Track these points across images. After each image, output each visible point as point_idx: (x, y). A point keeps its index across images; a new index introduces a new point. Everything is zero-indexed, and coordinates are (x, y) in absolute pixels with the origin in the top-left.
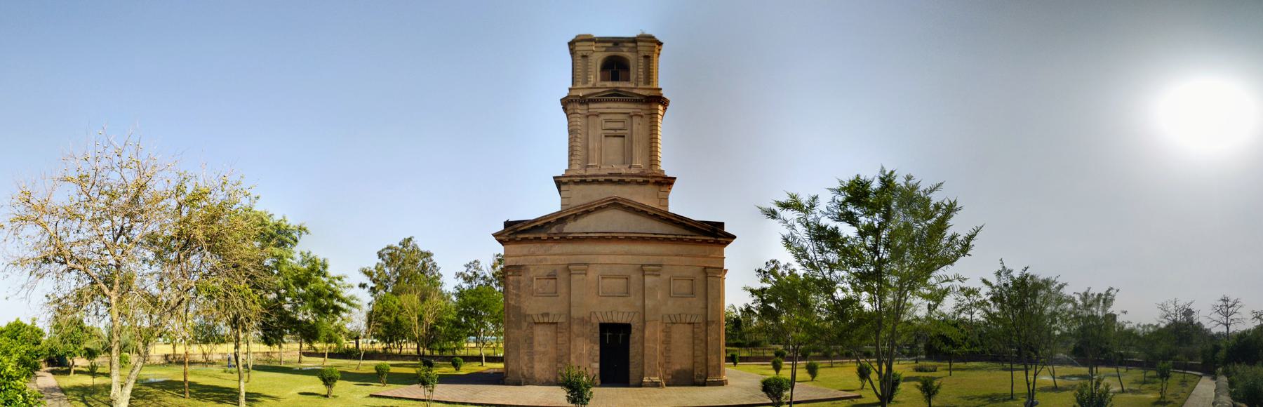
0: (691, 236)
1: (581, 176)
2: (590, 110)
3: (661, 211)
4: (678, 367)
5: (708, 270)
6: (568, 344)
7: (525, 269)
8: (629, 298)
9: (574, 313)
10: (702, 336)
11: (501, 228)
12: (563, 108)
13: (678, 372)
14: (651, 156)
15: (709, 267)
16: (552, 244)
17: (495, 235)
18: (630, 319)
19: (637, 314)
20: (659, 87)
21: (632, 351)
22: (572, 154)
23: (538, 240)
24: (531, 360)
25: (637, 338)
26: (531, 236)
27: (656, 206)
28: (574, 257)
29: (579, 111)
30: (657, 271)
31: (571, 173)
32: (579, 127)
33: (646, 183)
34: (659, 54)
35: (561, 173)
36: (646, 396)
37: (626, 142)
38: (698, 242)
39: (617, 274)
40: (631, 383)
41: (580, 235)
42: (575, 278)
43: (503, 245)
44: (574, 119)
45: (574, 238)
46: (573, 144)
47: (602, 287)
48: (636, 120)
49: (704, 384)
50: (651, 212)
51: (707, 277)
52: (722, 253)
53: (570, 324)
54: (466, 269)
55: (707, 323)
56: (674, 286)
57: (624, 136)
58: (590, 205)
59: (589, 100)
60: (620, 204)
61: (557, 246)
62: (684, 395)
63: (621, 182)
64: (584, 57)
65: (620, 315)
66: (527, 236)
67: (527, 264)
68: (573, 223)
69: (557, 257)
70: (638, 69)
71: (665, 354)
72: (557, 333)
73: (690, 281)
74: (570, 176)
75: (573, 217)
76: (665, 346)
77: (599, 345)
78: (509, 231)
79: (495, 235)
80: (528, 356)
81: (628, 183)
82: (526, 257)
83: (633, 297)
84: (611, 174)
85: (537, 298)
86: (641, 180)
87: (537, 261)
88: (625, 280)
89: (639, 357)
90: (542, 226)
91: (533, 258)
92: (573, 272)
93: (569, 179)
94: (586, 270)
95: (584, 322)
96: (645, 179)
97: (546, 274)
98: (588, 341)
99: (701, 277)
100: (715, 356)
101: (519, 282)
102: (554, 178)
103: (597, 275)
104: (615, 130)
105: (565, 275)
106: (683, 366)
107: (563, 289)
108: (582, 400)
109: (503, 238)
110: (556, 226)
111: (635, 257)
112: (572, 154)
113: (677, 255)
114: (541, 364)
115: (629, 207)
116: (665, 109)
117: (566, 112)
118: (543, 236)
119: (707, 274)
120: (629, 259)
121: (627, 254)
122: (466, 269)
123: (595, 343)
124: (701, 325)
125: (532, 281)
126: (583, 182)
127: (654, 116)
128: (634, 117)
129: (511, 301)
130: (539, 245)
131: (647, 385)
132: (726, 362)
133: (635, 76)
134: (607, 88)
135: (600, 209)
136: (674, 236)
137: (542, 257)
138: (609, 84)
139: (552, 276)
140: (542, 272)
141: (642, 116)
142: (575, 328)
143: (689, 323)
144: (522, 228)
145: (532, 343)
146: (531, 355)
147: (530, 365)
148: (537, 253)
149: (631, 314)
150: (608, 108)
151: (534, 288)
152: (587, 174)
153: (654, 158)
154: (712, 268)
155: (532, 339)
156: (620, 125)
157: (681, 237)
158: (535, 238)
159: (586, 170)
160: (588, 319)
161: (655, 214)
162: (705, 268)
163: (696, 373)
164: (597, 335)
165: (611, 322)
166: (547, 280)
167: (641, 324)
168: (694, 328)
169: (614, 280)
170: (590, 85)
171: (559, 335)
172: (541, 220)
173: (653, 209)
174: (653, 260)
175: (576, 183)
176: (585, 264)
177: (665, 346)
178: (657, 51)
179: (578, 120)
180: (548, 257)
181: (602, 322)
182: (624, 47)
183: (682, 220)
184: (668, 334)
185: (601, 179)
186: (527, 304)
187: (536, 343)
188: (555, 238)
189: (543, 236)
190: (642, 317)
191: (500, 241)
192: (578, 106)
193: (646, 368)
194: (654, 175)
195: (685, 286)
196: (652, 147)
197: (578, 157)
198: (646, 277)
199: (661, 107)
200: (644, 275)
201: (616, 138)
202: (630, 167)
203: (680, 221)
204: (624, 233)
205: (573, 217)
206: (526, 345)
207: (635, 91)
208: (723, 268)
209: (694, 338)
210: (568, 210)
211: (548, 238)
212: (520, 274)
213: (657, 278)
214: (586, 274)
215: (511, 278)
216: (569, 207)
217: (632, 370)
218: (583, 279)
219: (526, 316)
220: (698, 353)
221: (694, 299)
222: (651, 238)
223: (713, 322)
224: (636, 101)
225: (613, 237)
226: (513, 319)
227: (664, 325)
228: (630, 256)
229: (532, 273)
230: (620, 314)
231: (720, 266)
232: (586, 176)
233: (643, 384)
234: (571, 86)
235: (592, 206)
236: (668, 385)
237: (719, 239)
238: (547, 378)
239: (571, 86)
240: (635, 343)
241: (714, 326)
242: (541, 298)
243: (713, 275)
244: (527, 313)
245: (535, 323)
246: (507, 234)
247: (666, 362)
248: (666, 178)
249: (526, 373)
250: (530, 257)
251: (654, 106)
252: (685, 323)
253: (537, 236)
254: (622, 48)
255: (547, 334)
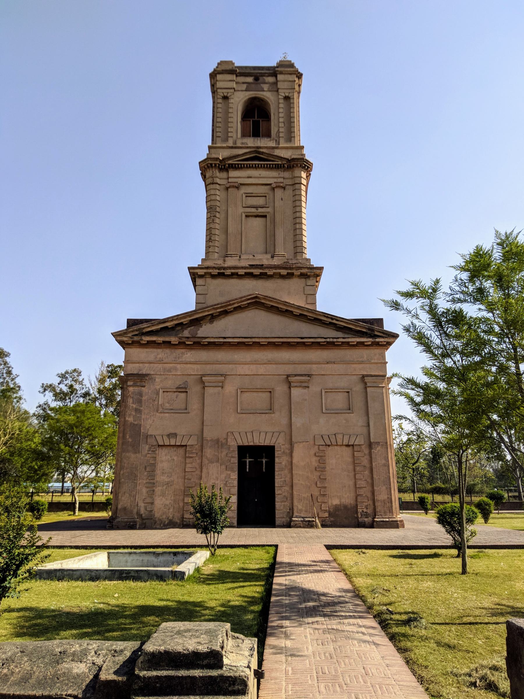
0: (343, 338)
1: (219, 268)
2: (230, 180)
3: (308, 310)
4: (336, 502)
5: (367, 379)
6: (198, 472)
7: (150, 379)
8: (273, 415)
9: (208, 434)
10: (365, 461)
11: (123, 326)
12: (202, 174)
13: (337, 508)
14: (295, 235)
15: (368, 376)
16: (183, 350)
17: (115, 335)
18: (274, 440)
19: (282, 434)
20: (301, 145)
21: (278, 481)
22: (210, 239)
23: (167, 344)
24: (152, 493)
25: (283, 463)
26: (160, 339)
27: (302, 304)
28: (208, 366)
29: (218, 181)
30: (305, 382)
31: (209, 264)
32: (218, 204)
33: (290, 276)
34: (299, 93)
35: (196, 262)
36: (295, 535)
37: (268, 223)
38: (353, 346)
39: (259, 387)
40: (278, 522)
41: (216, 340)
42: (209, 391)
43: (124, 348)
44: (212, 192)
45: (210, 343)
46: (212, 226)
47: (241, 402)
48: (279, 193)
49: (372, 526)
50: (297, 312)
51: (366, 388)
52: (384, 357)
53: (202, 446)
54: (59, 379)
55: (370, 445)
56: (326, 399)
57: (265, 216)
58: (228, 303)
59: (229, 164)
60: (263, 303)
61: (189, 354)
62: (344, 535)
63: (263, 276)
64: (225, 98)
65: (263, 435)
66: (154, 338)
67: (152, 373)
68: (209, 326)
69: (189, 366)
70: (279, 117)
71: (319, 485)
72: (186, 458)
73: (346, 394)
74: (207, 268)
75: (209, 318)
76: (318, 474)
77: (237, 472)
78: (133, 331)
79: (115, 335)
80: (147, 487)
81: (271, 277)
82: (152, 365)
83: (277, 414)
84: (252, 266)
85: (162, 415)
86: (284, 272)
87: (165, 369)
88: (268, 394)
89: (287, 488)
90: (173, 328)
91: (160, 366)
92: (206, 384)
93: (205, 271)
94: (222, 382)
95: (218, 444)
96: (289, 271)
97: (176, 386)
98: (223, 467)
99: (358, 388)
100: (384, 488)
101: (141, 394)
102: (189, 268)
103: (235, 388)
104: (256, 207)
105: (198, 388)
106: (343, 500)
107: (194, 405)
108: (215, 528)
109: (125, 339)
110: (189, 329)
111: (280, 366)
112: (210, 239)
113: (328, 363)
114: (164, 499)
115: (272, 306)
116: (308, 177)
117: (204, 181)
118: (174, 340)
119: (366, 384)
120: (272, 369)
121: (269, 362)
122: (59, 379)
123: (232, 470)
124: (363, 447)
125: (158, 394)
126: (221, 275)
127: (297, 186)
128: (276, 190)
129: (129, 417)
130: (168, 351)
131: (296, 526)
132: (400, 510)
133: (276, 130)
134: (248, 148)
135: (239, 309)
136: (323, 340)
137: (171, 365)
138: (251, 142)
139: (182, 389)
140: (170, 383)
141: (284, 188)
142: (209, 452)
143: (348, 446)
144: (149, 329)
145: (154, 471)
146: (152, 486)
147: (149, 500)
148: (165, 361)
149: (276, 434)
150: (248, 177)
151: (160, 403)
152: (226, 266)
153: (298, 244)
154: (372, 376)
155: (154, 465)
156: (261, 201)
157: (331, 340)
158: (164, 342)
159: (225, 261)
160: (224, 441)
161: (301, 315)
162: (363, 376)
163: (360, 510)
164: (235, 460)
165: (251, 444)
166: (176, 394)
167: (287, 446)
168: (354, 451)
169: (255, 394)
170: (230, 143)
171: (188, 460)
172: (172, 321)
173: (299, 307)
174: (301, 369)
175: (213, 277)
176: (222, 375)
177: (318, 474)
178: (296, 87)
179: (218, 193)
180: (178, 366)
181: (241, 444)
182: (265, 83)
183: (332, 319)
184: (321, 458)
185: (241, 272)
186: (150, 422)
187: (158, 472)
188: (187, 343)
189: (174, 340)
190: (288, 438)
191: (122, 343)
192: (218, 174)
193: (296, 503)
194: (299, 265)
195: (340, 401)
196: (295, 229)
197: (217, 244)
198: (292, 389)
199: (304, 175)
200: (290, 388)
201: (258, 219)
202: (272, 257)
203: (330, 320)
204: (266, 338)
205: (209, 318)
206: (146, 473)
207: (277, 153)
208: (385, 376)
209: (354, 463)
210: (202, 309)
211: (179, 342)
212: (144, 384)
213: (306, 391)
214: (222, 387)
215: (131, 389)
216: (204, 305)
217: (279, 505)
218: (219, 393)
219: (147, 437)
220: (361, 483)
221: (352, 415)
222: (298, 343)
223: (378, 443)
224: (278, 167)
225: (254, 342)
226: (130, 440)
227: (316, 447)
228: (274, 366)
229: (158, 383)
230: (261, 433)
231: (381, 374)
232: (224, 268)
233: (292, 524)
234: (210, 144)
235: (230, 305)
236: (324, 526)
237: (378, 340)
238: (171, 517)
239: (210, 144)
240: (282, 470)
241: (379, 448)
242: (167, 415)
243: (375, 385)
244: (149, 434)
245: (159, 445)
246: (130, 335)
247: (321, 495)
248: (312, 268)
249: (142, 511)
250: (156, 365)
251: (296, 172)
252: (343, 445)
253: (167, 339)
254: (262, 85)
255: (174, 460)
